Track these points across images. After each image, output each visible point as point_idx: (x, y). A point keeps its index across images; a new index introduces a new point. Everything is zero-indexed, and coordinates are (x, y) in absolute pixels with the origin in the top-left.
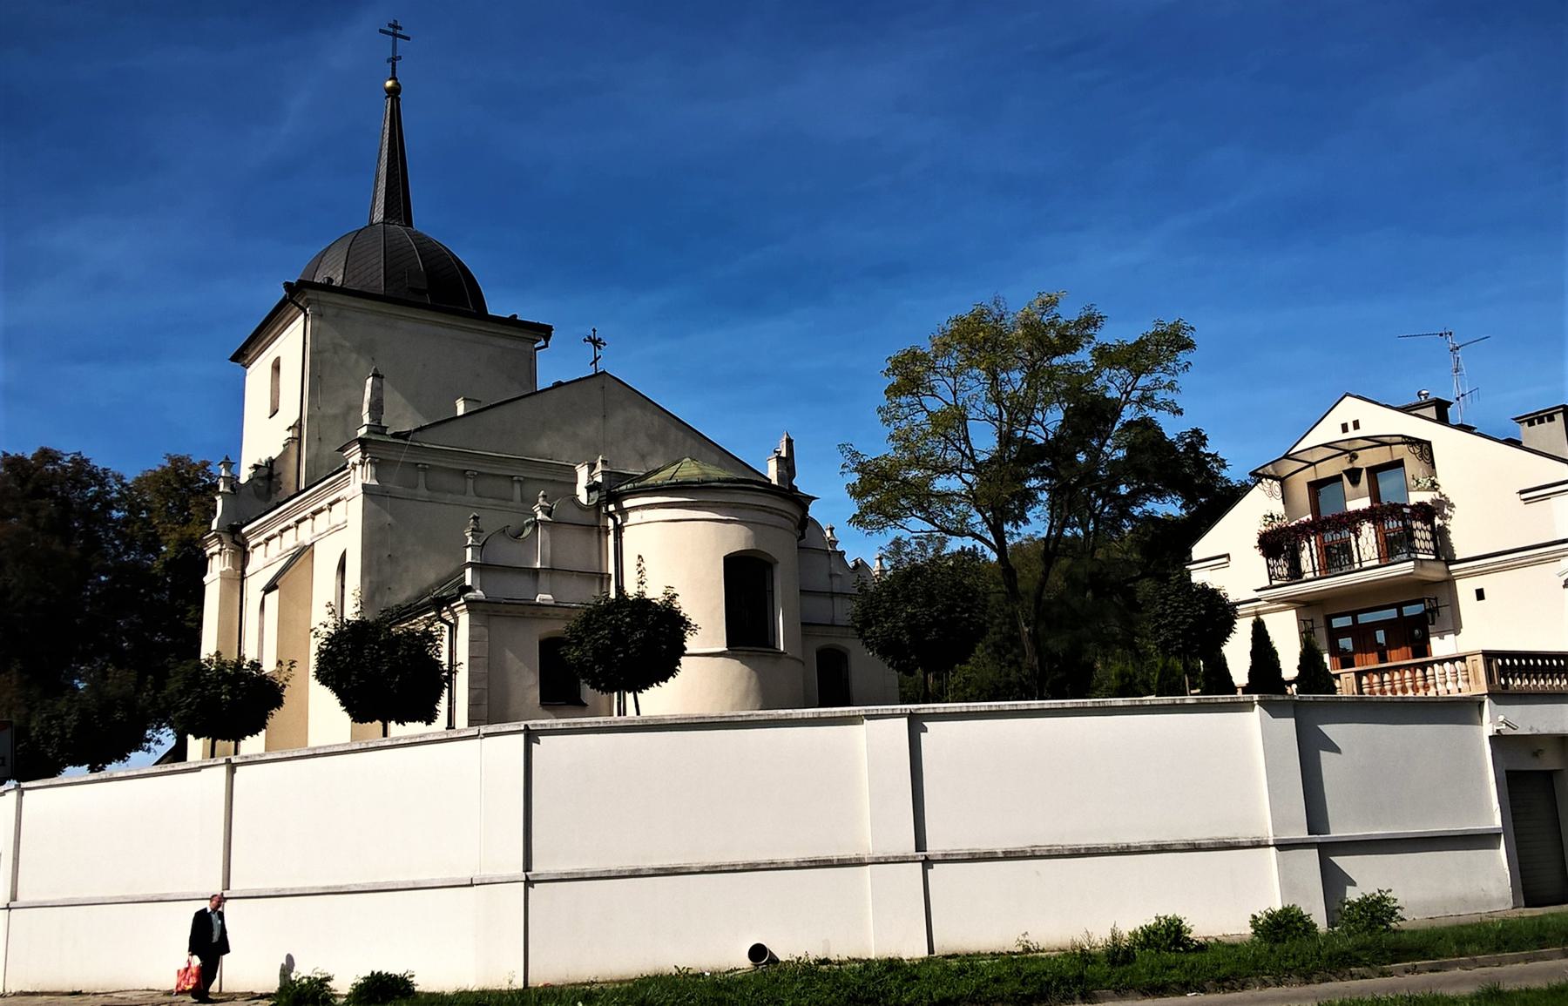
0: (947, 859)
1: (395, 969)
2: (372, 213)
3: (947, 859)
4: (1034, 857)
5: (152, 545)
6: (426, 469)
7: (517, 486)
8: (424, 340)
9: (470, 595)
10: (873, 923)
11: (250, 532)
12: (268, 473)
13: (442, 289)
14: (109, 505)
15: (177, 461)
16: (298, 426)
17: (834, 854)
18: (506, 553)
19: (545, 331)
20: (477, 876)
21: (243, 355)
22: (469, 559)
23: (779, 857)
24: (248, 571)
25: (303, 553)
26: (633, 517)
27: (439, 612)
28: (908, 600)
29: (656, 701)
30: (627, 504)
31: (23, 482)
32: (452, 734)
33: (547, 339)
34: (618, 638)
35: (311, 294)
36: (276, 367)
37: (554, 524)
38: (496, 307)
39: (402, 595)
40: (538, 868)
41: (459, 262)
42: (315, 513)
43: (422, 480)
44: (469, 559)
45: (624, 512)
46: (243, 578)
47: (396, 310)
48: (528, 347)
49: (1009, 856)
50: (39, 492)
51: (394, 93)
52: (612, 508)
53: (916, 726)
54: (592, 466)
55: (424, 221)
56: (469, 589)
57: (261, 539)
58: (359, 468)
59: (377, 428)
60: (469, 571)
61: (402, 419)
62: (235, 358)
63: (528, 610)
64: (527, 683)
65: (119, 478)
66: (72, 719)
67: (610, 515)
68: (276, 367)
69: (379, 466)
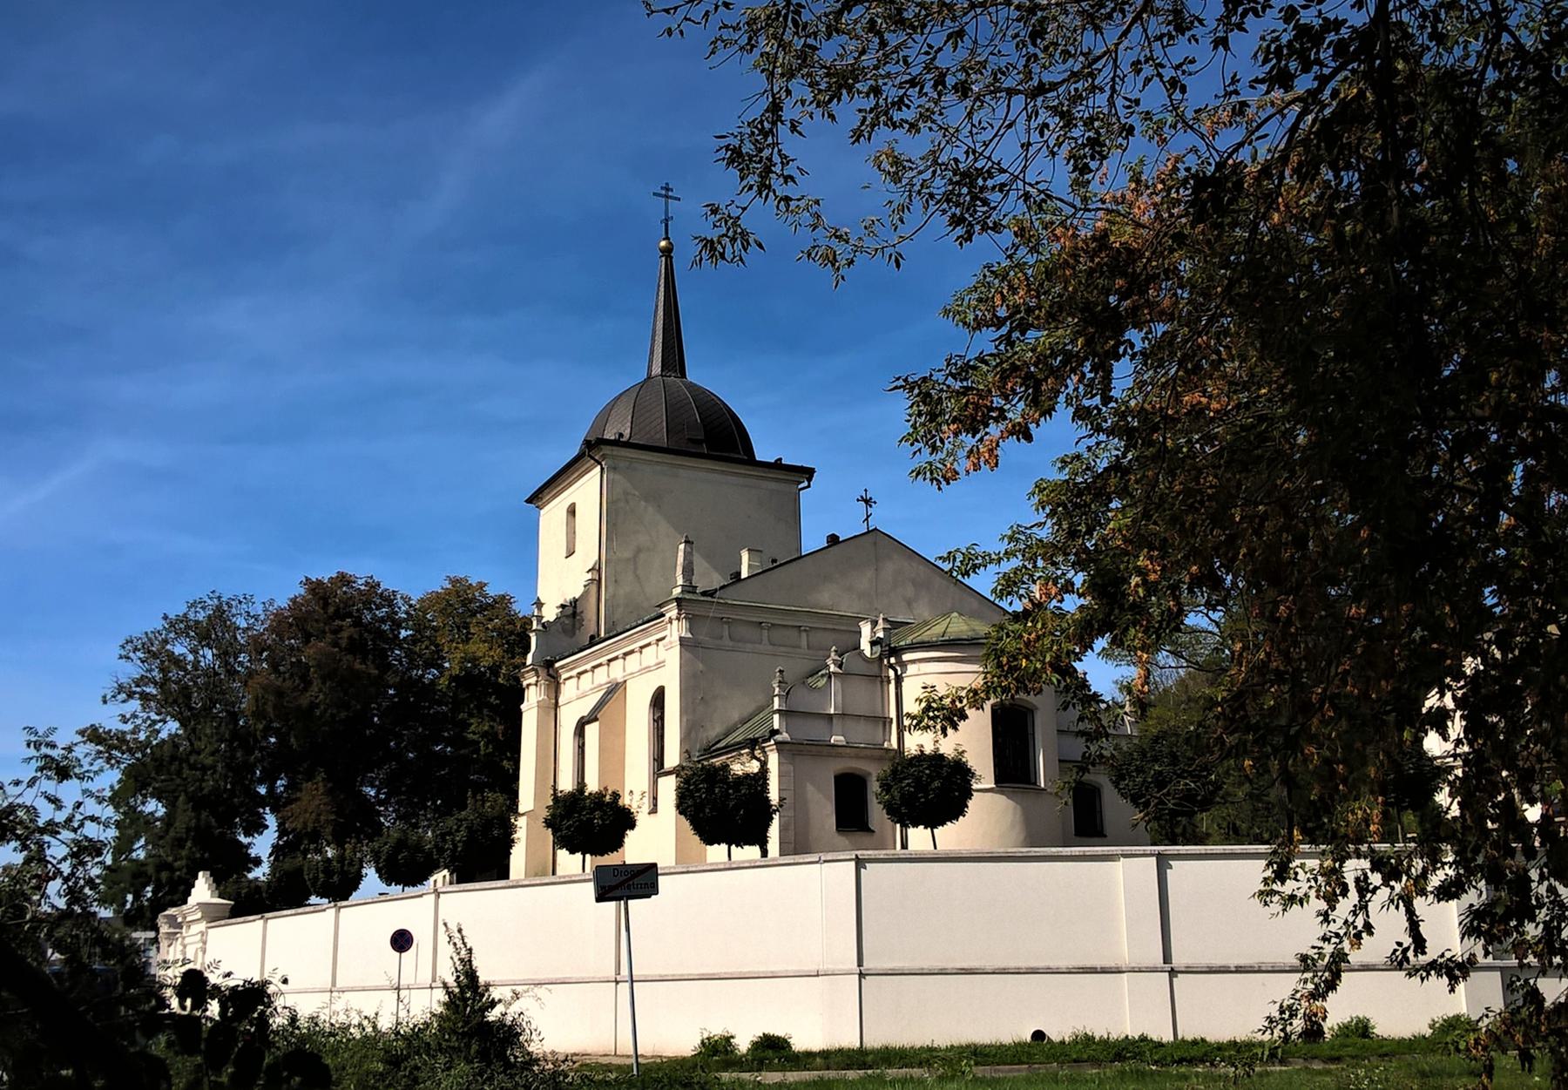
0: (1189, 971)
1: (778, 1032)
2: (650, 367)
3: (1189, 971)
4: (1260, 971)
5: (435, 661)
6: (730, 622)
7: (804, 635)
8: (704, 483)
9: (778, 737)
10: (1131, 1012)
11: (562, 667)
12: (572, 611)
13: (715, 437)
14: (398, 625)
15: (455, 582)
16: (596, 569)
17: (1098, 964)
18: (804, 701)
19: (808, 473)
20: (822, 968)
21: (538, 498)
22: (776, 707)
23: (1053, 964)
24: (561, 701)
25: (615, 690)
26: (911, 669)
27: (753, 750)
28: (1155, 760)
29: (950, 836)
30: (906, 657)
31: (326, 605)
32: (764, 861)
33: (809, 480)
34: (921, 786)
35: (606, 450)
36: (572, 511)
37: (845, 675)
38: (763, 453)
39: (713, 732)
40: (867, 964)
41: (729, 410)
42: (626, 654)
43: (726, 633)
44: (776, 707)
45: (904, 665)
46: (556, 705)
47: (679, 460)
48: (793, 488)
49: (1239, 970)
50: (339, 615)
51: (667, 252)
52: (893, 660)
53: (1163, 863)
54: (874, 623)
55: (698, 373)
56: (777, 732)
57: (574, 673)
58: (675, 623)
59: (689, 588)
60: (776, 717)
61: (709, 578)
62: (529, 501)
63: (825, 750)
64: (824, 810)
65: (406, 600)
66: (461, 835)
67: (891, 666)
68: (572, 511)
69: (692, 620)
